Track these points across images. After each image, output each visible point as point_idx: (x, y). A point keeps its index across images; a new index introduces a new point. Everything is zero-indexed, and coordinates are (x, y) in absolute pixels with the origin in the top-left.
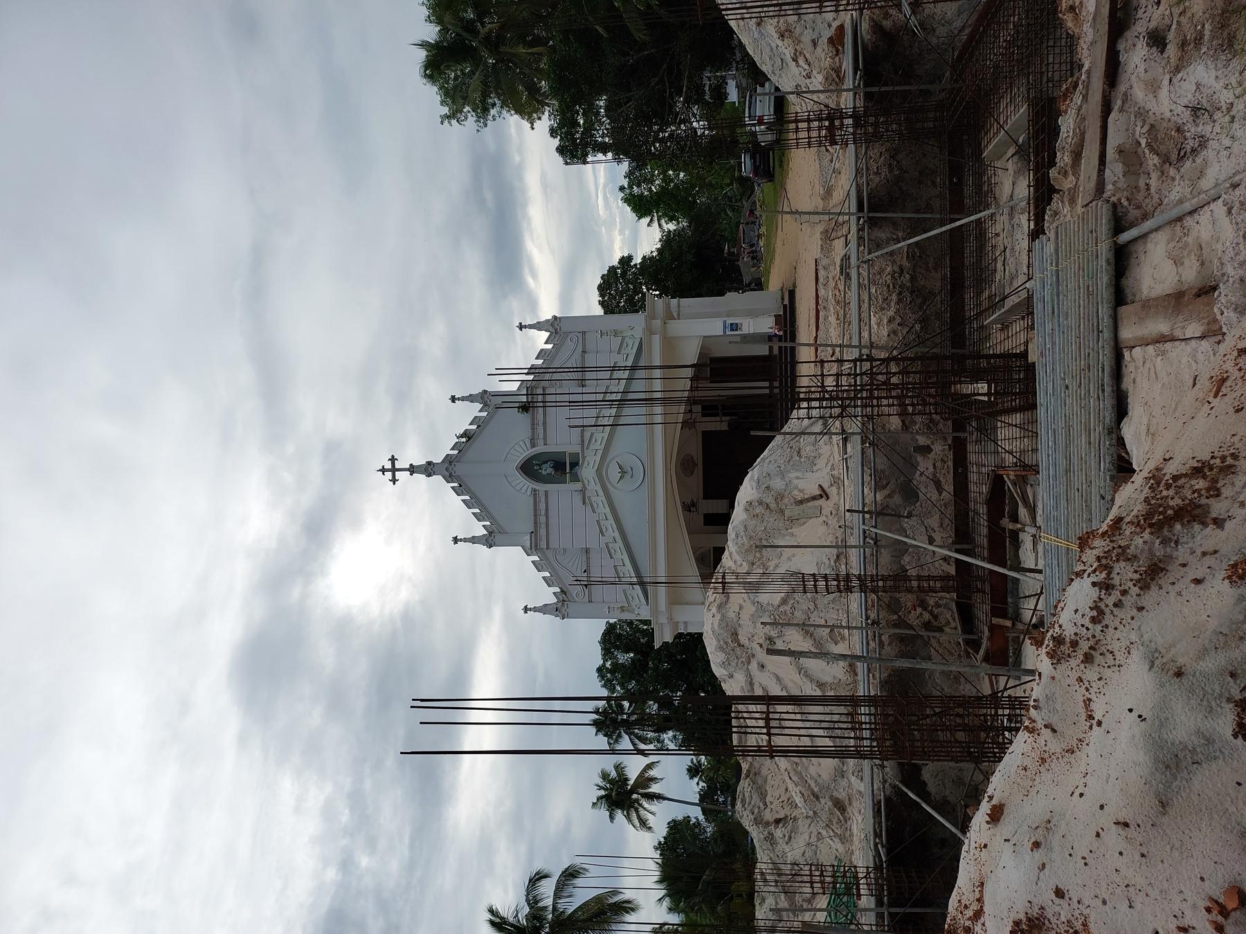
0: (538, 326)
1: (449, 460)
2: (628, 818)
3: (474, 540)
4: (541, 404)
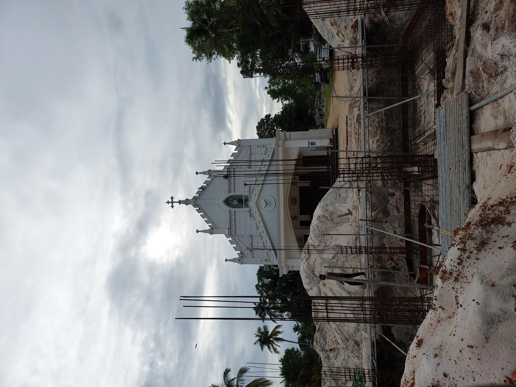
0: (232, 143)
2: (269, 348)
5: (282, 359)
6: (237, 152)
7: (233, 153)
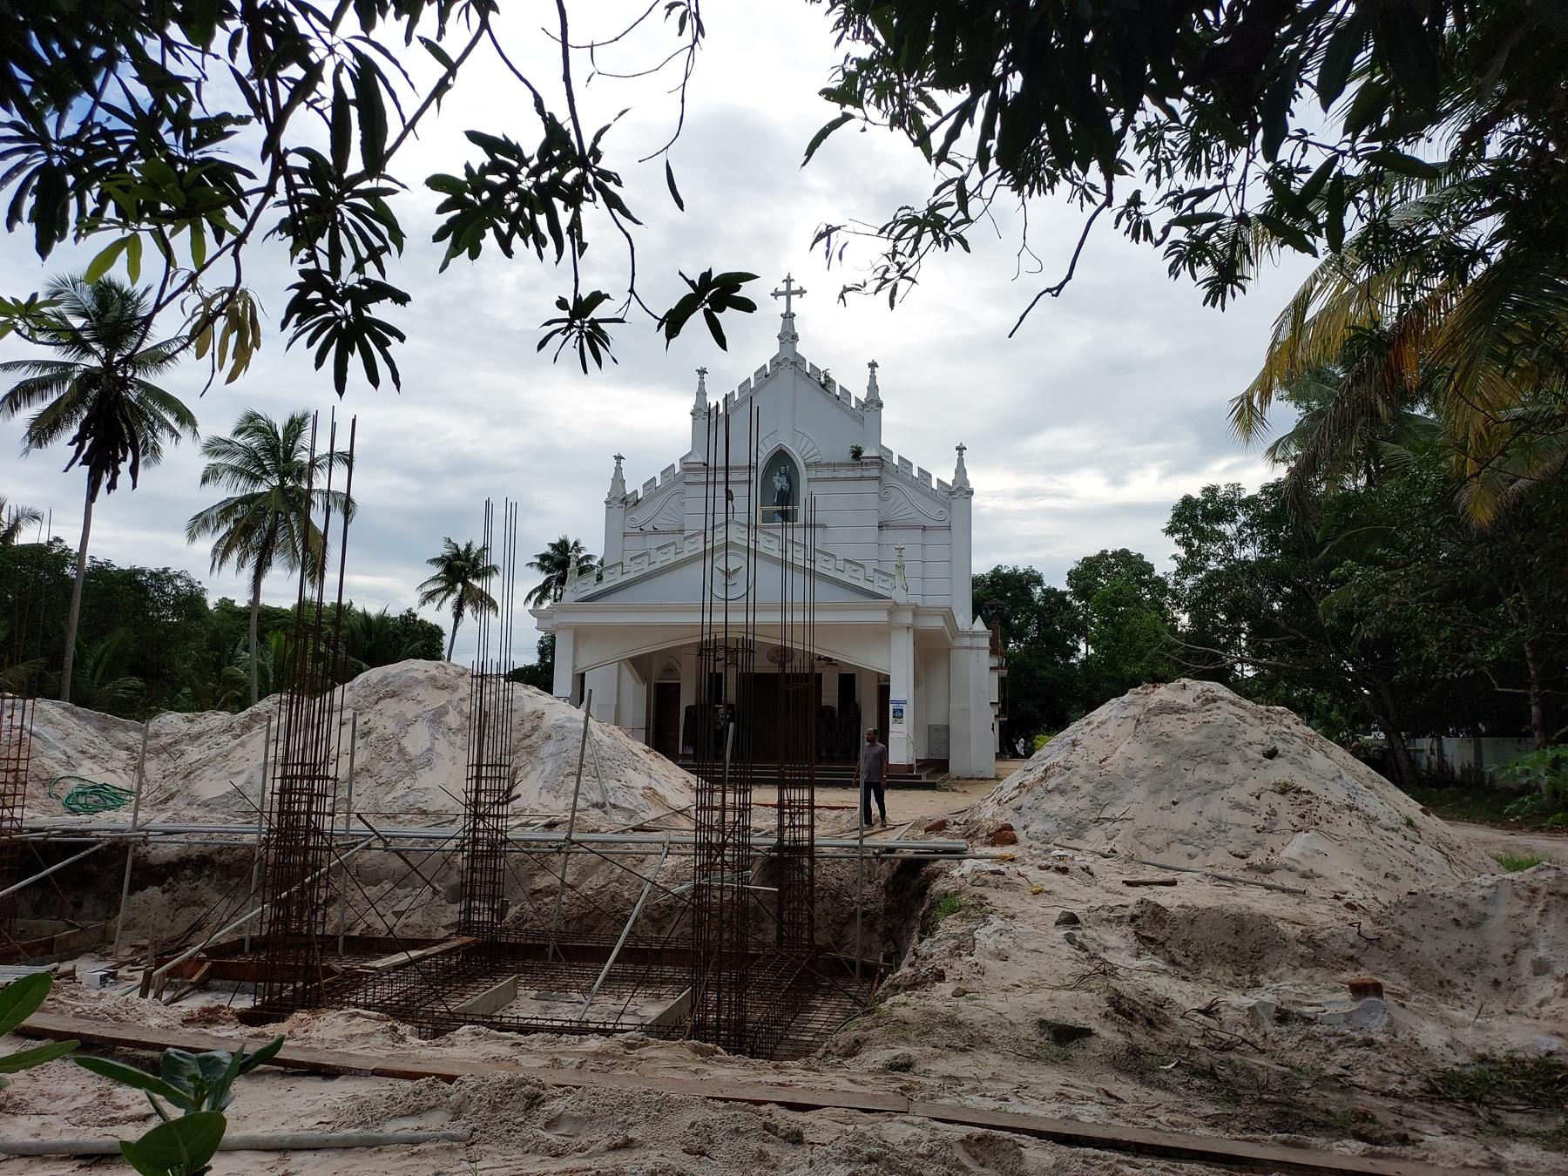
0: (961, 471)
1: (798, 361)
2: (435, 579)
3: (701, 393)
4: (711, 478)
5: (415, 615)
6: (916, 474)
7: (930, 476)
